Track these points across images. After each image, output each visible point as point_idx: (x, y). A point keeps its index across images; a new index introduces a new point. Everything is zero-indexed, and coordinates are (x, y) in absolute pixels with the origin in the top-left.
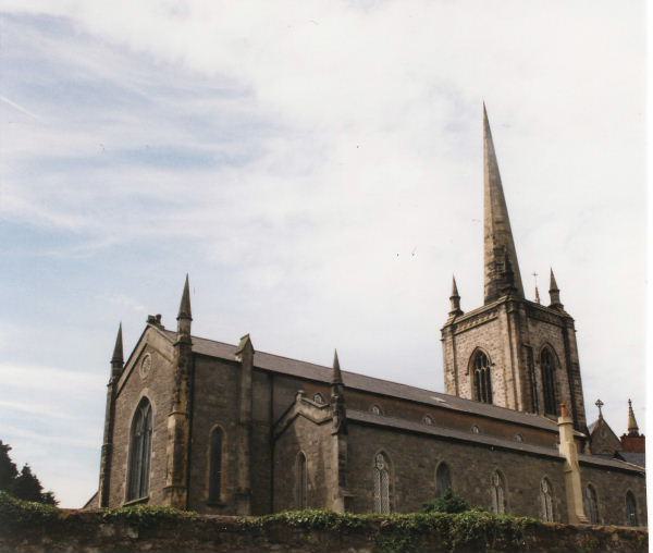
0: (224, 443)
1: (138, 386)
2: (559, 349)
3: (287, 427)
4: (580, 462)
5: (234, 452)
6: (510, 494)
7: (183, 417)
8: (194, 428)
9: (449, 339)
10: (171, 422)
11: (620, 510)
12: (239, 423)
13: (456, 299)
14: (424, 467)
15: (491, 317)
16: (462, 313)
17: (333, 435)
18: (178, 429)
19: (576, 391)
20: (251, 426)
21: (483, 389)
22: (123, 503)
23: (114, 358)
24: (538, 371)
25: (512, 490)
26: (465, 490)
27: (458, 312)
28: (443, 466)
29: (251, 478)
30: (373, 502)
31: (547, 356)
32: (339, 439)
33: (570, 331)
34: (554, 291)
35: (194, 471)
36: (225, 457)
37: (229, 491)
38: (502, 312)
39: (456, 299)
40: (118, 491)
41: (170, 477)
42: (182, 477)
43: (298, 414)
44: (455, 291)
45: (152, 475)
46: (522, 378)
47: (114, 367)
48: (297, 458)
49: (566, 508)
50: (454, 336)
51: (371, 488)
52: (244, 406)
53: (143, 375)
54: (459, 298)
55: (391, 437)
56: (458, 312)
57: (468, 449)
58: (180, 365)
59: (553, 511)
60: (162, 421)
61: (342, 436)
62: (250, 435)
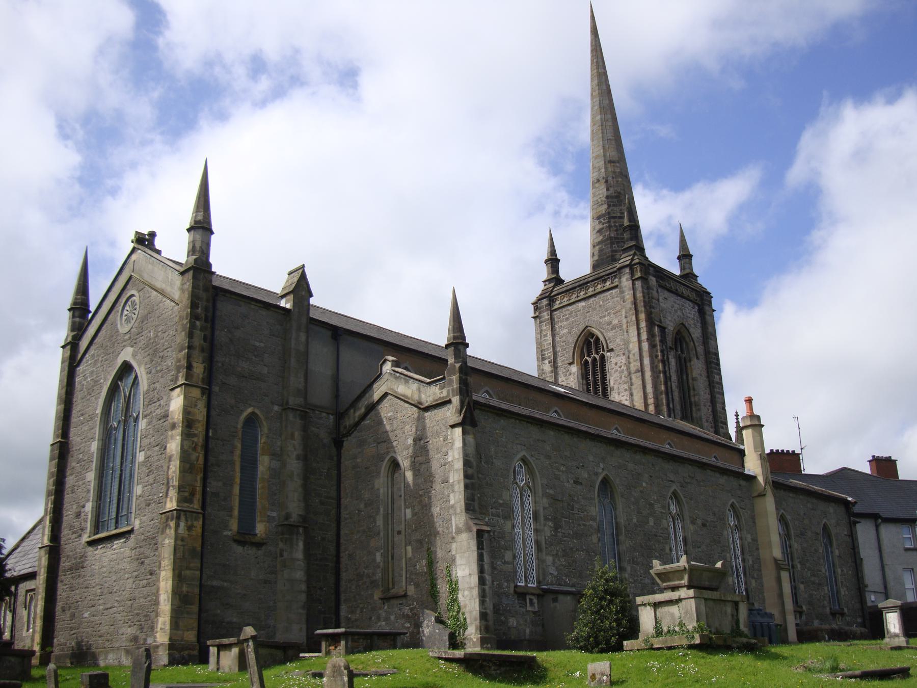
0: (262, 440)
1: (116, 343)
2: (696, 333)
3: (363, 417)
4: (773, 482)
5: (277, 455)
6: (691, 527)
7: (196, 393)
8: (213, 413)
9: (546, 315)
10: (176, 403)
11: (816, 551)
12: (286, 408)
13: (553, 261)
14: (581, 484)
15: (608, 284)
16: (562, 281)
17: (453, 426)
18: (187, 411)
19: (717, 390)
20: (305, 413)
21: (595, 382)
22: (85, 538)
23: (75, 303)
24: (673, 361)
25: (693, 522)
26: (635, 520)
27: (555, 279)
28: (605, 482)
29: (307, 492)
30: (513, 541)
31: (680, 339)
32: (464, 433)
33: (707, 308)
34: (685, 257)
35: (214, 485)
36: (264, 464)
37: (270, 519)
38: (624, 279)
39: (553, 261)
40: (78, 515)
41: (173, 493)
42: (193, 494)
43: (386, 395)
44: (553, 252)
45: (138, 490)
46: (653, 368)
47: (74, 316)
48: (385, 464)
49: (757, 549)
50: (552, 311)
51: (509, 515)
52: (296, 381)
53: (123, 328)
54: (558, 261)
55: (535, 432)
56: (555, 279)
57: (31, 537)
58: (194, 305)
59: (743, 553)
60: (156, 399)
61: (468, 428)
62: (305, 429)
